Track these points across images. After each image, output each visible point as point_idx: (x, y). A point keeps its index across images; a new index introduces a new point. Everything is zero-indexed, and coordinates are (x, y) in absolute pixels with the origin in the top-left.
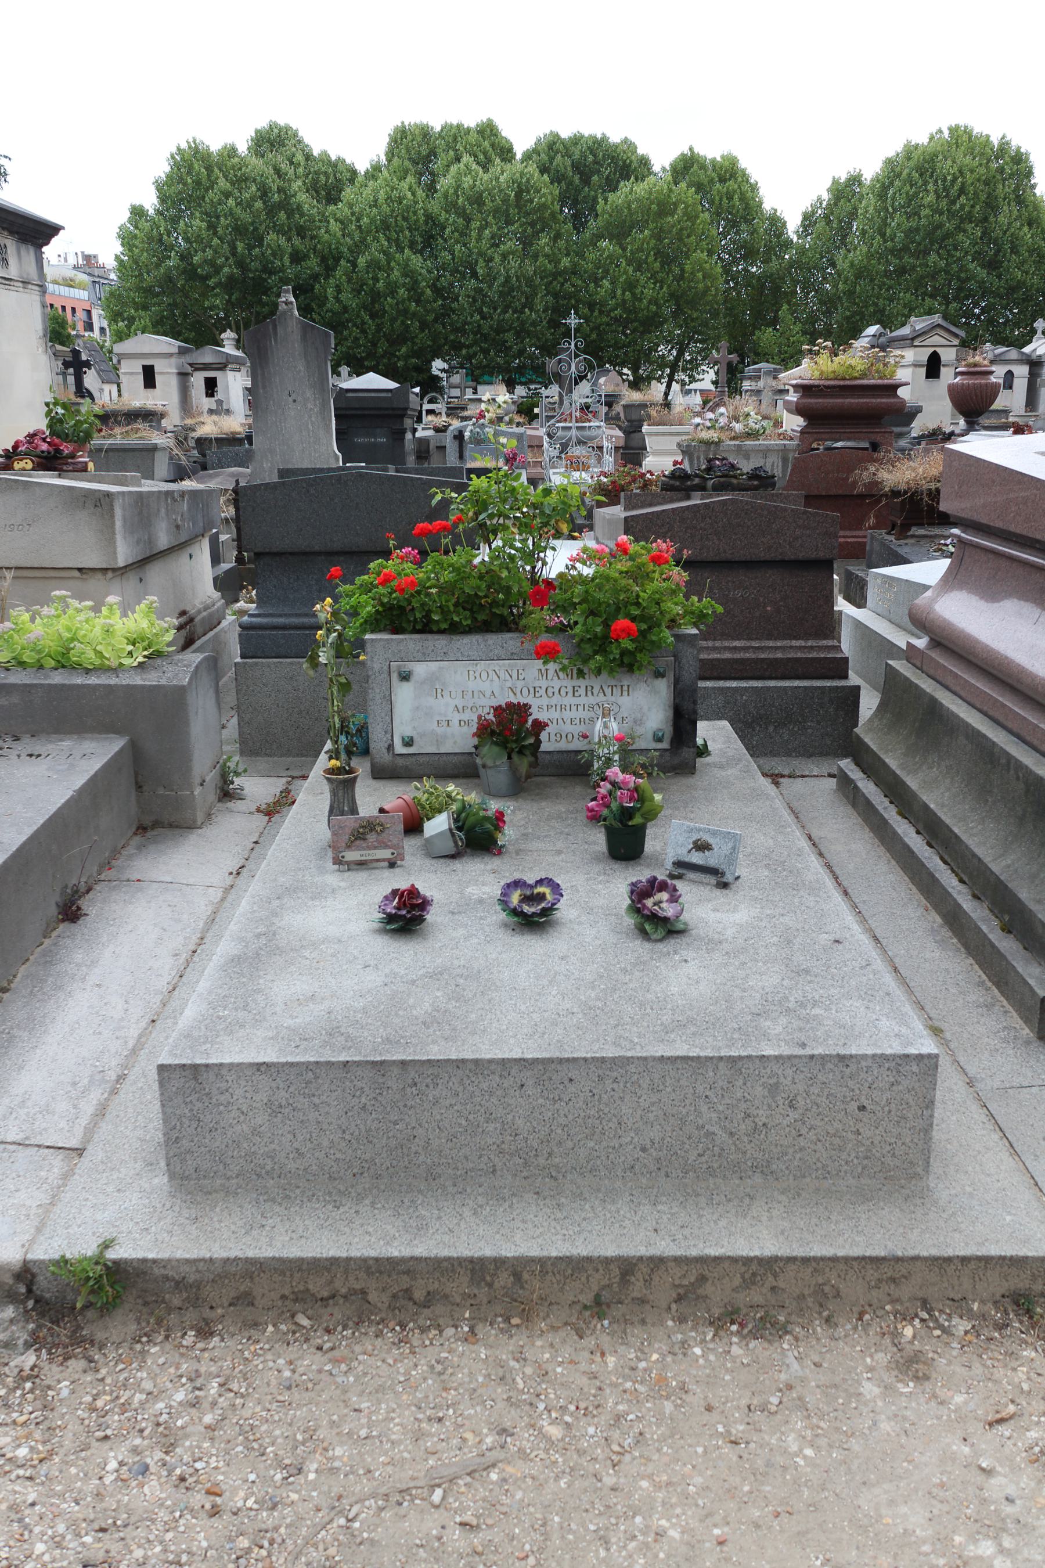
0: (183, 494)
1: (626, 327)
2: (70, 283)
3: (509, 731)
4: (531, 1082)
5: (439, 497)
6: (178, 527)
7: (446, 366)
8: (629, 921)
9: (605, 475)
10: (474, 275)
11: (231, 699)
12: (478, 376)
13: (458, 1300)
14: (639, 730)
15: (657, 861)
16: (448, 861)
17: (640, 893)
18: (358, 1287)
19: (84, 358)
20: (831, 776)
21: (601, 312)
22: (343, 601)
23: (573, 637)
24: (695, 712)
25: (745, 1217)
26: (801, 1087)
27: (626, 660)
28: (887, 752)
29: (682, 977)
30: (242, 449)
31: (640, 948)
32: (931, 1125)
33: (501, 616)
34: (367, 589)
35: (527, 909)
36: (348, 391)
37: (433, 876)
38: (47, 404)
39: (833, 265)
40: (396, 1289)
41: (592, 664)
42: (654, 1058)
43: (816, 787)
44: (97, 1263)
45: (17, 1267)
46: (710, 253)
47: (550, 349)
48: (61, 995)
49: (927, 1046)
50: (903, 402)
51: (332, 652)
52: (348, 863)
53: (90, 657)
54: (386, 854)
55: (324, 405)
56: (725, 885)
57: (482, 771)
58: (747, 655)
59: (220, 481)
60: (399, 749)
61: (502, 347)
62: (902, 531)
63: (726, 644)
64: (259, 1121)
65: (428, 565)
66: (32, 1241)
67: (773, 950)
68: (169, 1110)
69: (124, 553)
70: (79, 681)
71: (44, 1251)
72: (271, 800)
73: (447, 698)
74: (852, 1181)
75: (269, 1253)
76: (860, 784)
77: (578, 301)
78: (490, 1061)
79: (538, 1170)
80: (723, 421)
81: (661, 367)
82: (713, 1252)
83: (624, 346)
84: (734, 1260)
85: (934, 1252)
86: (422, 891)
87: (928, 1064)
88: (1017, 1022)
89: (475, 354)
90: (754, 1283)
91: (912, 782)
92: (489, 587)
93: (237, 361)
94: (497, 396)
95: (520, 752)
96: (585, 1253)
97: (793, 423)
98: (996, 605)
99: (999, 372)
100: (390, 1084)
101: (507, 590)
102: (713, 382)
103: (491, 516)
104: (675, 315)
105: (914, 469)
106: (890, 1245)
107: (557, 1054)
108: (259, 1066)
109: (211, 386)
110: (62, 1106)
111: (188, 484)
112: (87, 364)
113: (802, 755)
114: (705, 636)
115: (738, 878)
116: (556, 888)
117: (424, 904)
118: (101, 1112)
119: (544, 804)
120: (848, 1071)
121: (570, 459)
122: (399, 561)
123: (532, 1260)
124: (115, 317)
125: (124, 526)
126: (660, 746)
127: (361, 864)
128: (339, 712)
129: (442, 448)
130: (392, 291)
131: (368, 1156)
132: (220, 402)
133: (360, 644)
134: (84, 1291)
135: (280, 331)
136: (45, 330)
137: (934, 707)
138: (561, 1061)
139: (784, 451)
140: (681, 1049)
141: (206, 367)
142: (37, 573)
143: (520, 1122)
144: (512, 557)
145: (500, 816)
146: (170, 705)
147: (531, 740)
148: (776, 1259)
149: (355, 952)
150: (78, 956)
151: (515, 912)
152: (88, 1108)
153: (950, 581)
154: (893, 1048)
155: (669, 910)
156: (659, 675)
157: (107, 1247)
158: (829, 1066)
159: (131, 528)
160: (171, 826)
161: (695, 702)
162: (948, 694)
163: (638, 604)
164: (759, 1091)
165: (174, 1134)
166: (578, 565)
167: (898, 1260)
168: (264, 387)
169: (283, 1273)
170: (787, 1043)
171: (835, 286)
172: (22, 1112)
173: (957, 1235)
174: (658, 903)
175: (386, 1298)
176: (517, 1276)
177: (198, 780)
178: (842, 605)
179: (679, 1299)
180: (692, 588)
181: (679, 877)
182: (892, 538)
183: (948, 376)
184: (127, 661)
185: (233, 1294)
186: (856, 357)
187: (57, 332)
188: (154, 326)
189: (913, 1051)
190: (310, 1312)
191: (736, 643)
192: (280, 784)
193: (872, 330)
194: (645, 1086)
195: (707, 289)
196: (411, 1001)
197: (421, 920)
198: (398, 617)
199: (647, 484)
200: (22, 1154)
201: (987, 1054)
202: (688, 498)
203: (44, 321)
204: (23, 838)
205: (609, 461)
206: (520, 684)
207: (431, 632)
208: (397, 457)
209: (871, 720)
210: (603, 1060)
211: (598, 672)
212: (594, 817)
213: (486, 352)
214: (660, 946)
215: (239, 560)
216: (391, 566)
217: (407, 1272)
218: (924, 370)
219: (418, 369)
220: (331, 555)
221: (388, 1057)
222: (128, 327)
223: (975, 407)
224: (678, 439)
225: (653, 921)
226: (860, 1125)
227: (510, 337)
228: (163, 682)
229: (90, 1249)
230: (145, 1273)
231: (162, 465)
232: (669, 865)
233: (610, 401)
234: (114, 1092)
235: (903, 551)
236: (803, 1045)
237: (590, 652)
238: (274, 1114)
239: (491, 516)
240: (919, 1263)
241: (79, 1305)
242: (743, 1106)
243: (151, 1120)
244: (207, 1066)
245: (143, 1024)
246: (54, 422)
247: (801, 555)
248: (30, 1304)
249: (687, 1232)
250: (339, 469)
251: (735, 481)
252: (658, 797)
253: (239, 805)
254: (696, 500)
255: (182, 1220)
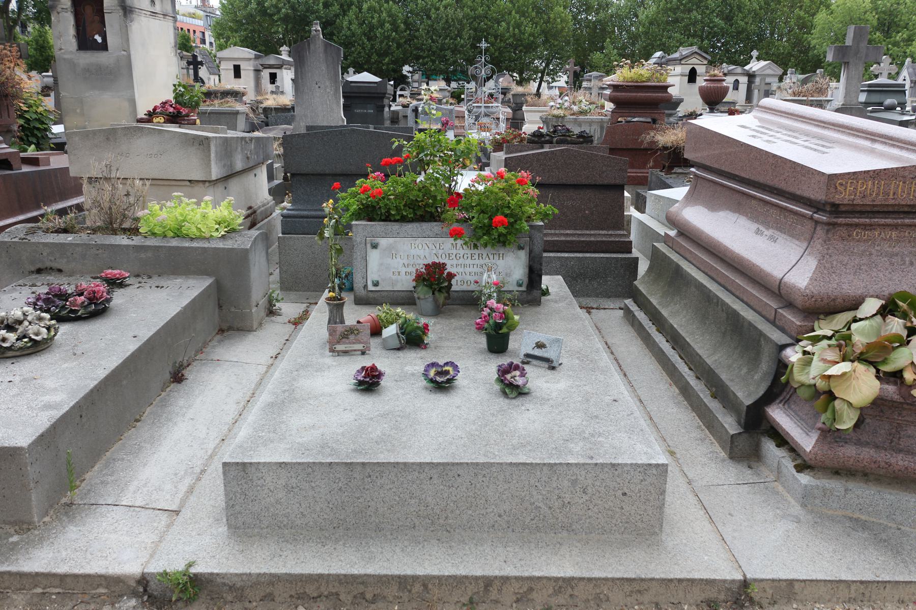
0: (251, 139)
1: (515, 49)
2: (193, 16)
3: (434, 278)
4: (436, 476)
5: (396, 144)
6: (248, 158)
7: (411, 69)
8: (497, 387)
9: (499, 134)
10: (429, 17)
11: (276, 258)
12: (429, 77)
13: (391, 599)
14: (509, 279)
15: (516, 354)
16: (396, 352)
17: (504, 371)
18: (334, 591)
19: (199, 59)
20: (620, 308)
21: (501, 40)
22: (340, 202)
23: (471, 225)
24: (541, 270)
25: (556, 555)
26: (590, 482)
27: (502, 239)
28: (652, 295)
29: (525, 418)
30: (289, 114)
31: (503, 402)
32: (664, 504)
33: (431, 212)
34: (354, 195)
35: (439, 379)
36: (352, 82)
37: (386, 360)
38: (174, 85)
39: (637, 16)
40: (356, 592)
41: (482, 241)
42: (507, 464)
43: (611, 316)
44: (184, 575)
45: (138, 577)
46: (565, 7)
47: (471, 61)
48: (170, 424)
49: (662, 459)
50: (671, 96)
51: (332, 231)
52: (338, 352)
53: (193, 231)
54: (360, 347)
55: (337, 90)
56: (553, 368)
57: (417, 301)
58: (574, 239)
59: (276, 132)
60: (371, 287)
61: (443, 58)
62: (669, 170)
63: (562, 232)
64: (280, 496)
65: (389, 182)
66: (148, 562)
67: (578, 404)
68: (229, 489)
69: (216, 172)
70: (187, 245)
71: (155, 568)
72: (297, 316)
73: (398, 259)
74: (619, 536)
75: (283, 571)
76: (636, 314)
77: (488, 34)
78: (413, 464)
79: (439, 527)
80: (566, 104)
81: (536, 72)
82: (537, 574)
83: (514, 61)
84: (549, 579)
85: (663, 576)
86: (379, 368)
87: (662, 469)
88: (718, 448)
89: (427, 63)
90: (560, 592)
91: (665, 313)
92: (424, 196)
93: (288, 63)
94: (437, 86)
95: (440, 291)
96: (464, 574)
97: (609, 106)
98: (713, 214)
99: (729, 81)
100: (355, 475)
101: (434, 198)
102: (567, 83)
103: (426, 155)
104: (545, 42)
105: (676, 135)
106: (638, 572)
107: (451, 460)
108: (281, 465)
109: (273, 77)
110: (168, 487)
111: (256, 134)
112: (201, 63)
113: (605, 297)
114: (546, 227)
115: (561, 364)
116: (456, 367)
117: (380, 375)
118: (191, 490)
119: (452, 320)
120: (616, 473)
121: (480, 125)
122: (372, 180)
123: (434, 577)
124: (218, 36)
125: (216, 156)
126: (520, 289)
127: (346, 352)
128: (335, 265)
129: (406, 117)
130: (382, 25)
131: (342, 517)
132: (278, 87)
133: (349, 227)
134: (177, 591)
135: (312, 46)
136: (176, 42)
137: (678, 269)
138: (453, 464)
139: (602, 121)
140: (522, 459)
141: (271, 67)
142: (174, 183)
143: (429, 499)
144: (437, 179)
145: (426, 327)
146: (240, 259)
147: (446, 284)
148: (573, 579)
149: (340, 402)
150: (181, 402)
151: (432, 381)
152: (183, 488)
153: (691, 198)
154: (643, 460)
155: (520, 381)
156: (521, 248)
157: (190, 566)
158: (606, 469)
159: (220, 158)
160: (238, 330)
161: (541, 264)
162: (686, 262)
163: (509, 207)
164: (566, 483)
165: (231, 503)
166: (476, 185)
167: (642, 580)
168: (302, 79)
169: (291, 583)
170: (582, 456)
171: (637, 29)
172: (145, 489)
173: (676, 567)
174: (513, 377)
175: (350, 598)
176: (425, 586)
177: (254, 304)
178: (632, 212)
179: (518, 601)
180: (541, 199)
181: (528, 363)
182: (663, 174)
183: (701, 82)
184: (215, 234)
185: (262, 594)
186: (644, 71)
187: (184, 44)
188: (242, 41)
189: (653, 462)
190: (306, 605)
191: (568, 232)
192: (303, 307)
193: (658, 54)
194: (501, 479)
195: (563, 28)
196: (370, 429)
197: (378, 384)
198: (371, 212)
199: (522, 140)
200: (144, 513)
201: (700, 466)
202: (542, 148)
203: (175, 38)
204: (152, 333)
205: (503, 126)
206: (440, 252)
207: (390, 221)
208: (378, 119)
209: (643, 277)
210: (477, 464)
211: (485, 246)
212: (480, 328)
213: (433, 62)
214: (514, 401)
215: (285, 178)
216: (369, 182)
217: (363, 583)
218: (687, 78)
219: (394, 71)
220: (335, 176)
221: (355, 461)
222: (226, 42)
223: (714, 100)
224: (541, 114)
225: (511, 388)
226: (623, 504)
227: (448, 53)
228: (235, 246)
229: (180, 566)
230: (212, 581)
231: (241, 122)
232: (522, 356)
233: (505, 91)
234: (199, 479)
235: (669, 181)
236: (592, 458)
237: (481, 234)
238: (289, 492)
239: (426, 155)
240: (654, 582)
241: (174, 599)
242: (557, 492)
243: (219, 495)
244: (251, 463)
245: (217, 441)
246: (178, 96)
247: (606, 182)
248: (145, 598)
249: (523, 563)
250: (344, 126)
251: (569, 139)
252: (516, 317)
253: (278, 319)
254: (547, 149)
255: (234, 551)
